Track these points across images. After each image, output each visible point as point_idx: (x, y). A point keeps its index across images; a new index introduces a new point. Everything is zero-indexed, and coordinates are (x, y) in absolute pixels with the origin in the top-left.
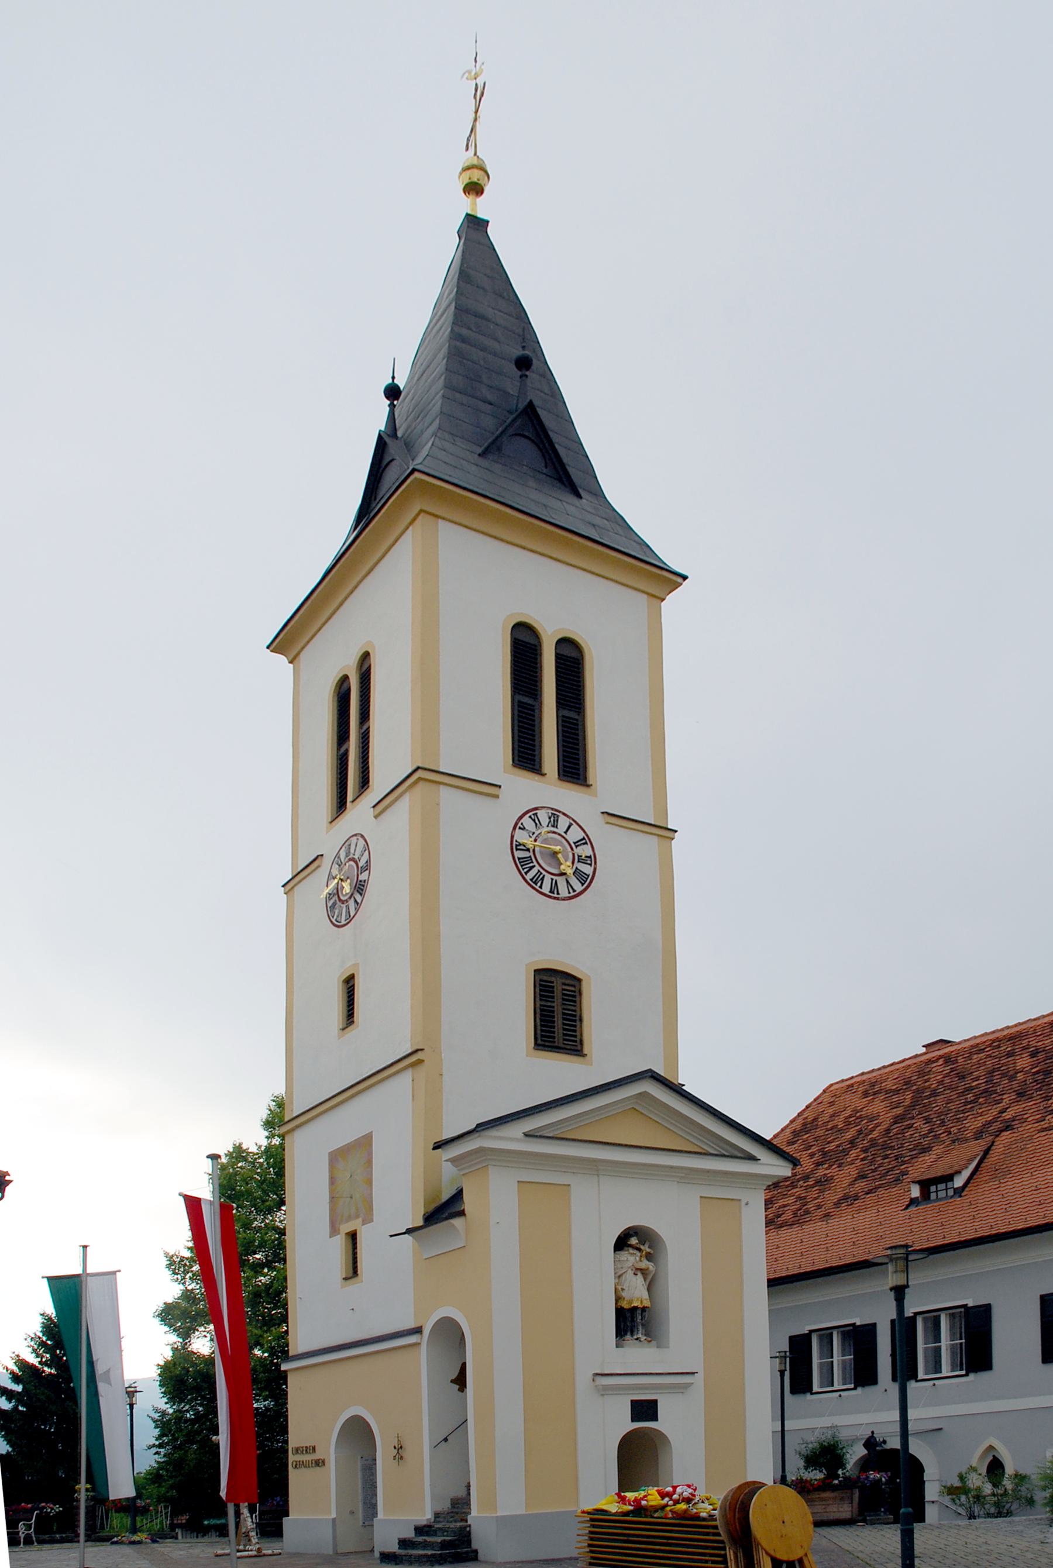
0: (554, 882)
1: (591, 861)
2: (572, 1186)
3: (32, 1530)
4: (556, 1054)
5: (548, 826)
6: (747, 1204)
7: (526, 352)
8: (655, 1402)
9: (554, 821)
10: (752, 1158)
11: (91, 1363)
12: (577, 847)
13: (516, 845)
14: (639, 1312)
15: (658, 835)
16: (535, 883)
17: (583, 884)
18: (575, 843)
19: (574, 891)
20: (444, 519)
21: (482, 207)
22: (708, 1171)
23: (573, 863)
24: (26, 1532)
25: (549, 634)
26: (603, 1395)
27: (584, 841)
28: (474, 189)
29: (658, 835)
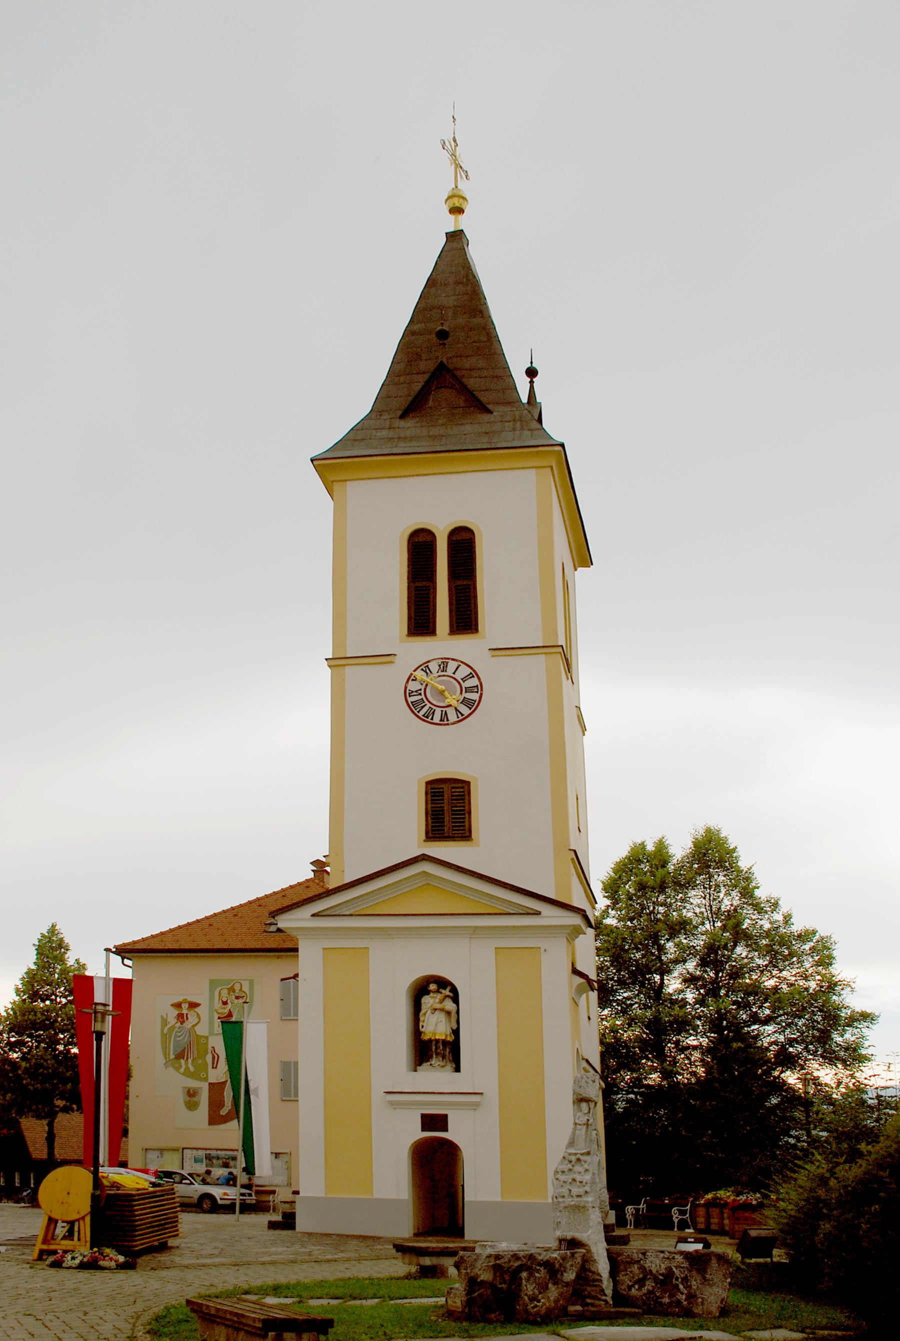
0: (444, 712)
1: (478, 689)
2: (370, 949)
3: (688, 1215)
4: (445, 843)
5: (438, 672)
6: (545, 950)
7: (444, 328)
8: (446, 1116)
9: (443, 667)
10: (538, 913)
11: (247, 1081)
12: (464, 682)
13: (409, 693)
14: (434, 1043)
15: (545, 653)
16: (427, 718)
17: (470, 709)
18: (462, 679)
19: (462, 715)
20: (350, 480)
21: (464, 223)
22: (514, 927)
23: (461, 693)
24: (680, 1217)
25: (441, 529)
26: (395, 1109)
27: (471, 675)
28: (457, 211)
29: (545, 653)
